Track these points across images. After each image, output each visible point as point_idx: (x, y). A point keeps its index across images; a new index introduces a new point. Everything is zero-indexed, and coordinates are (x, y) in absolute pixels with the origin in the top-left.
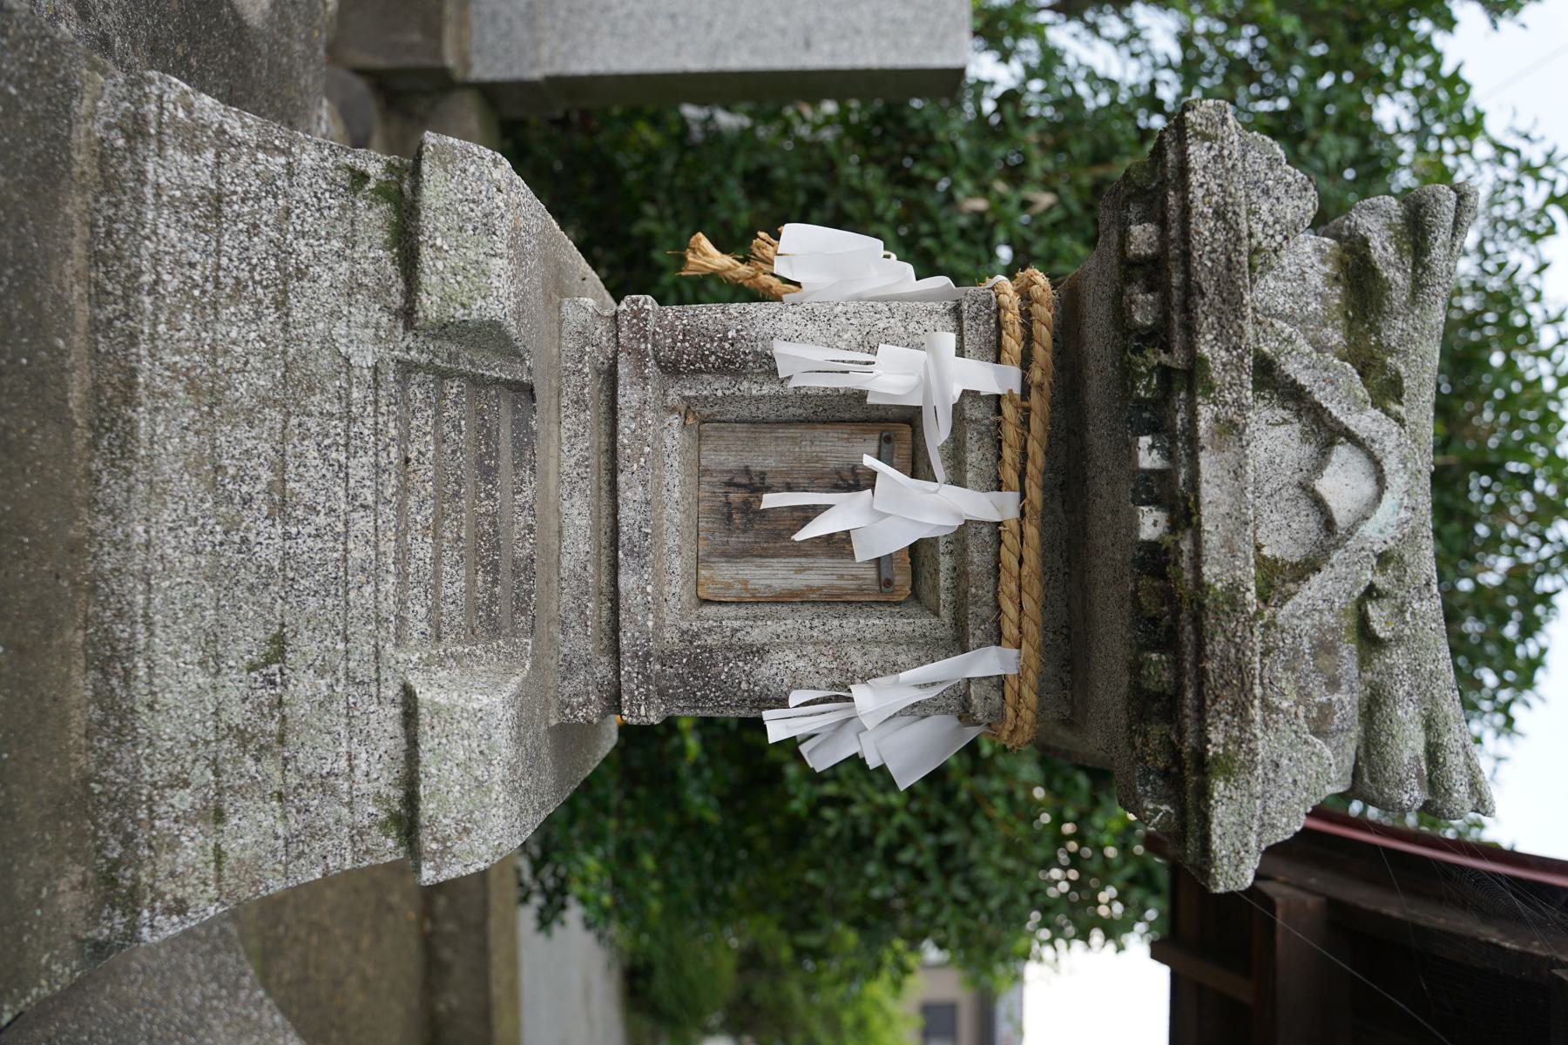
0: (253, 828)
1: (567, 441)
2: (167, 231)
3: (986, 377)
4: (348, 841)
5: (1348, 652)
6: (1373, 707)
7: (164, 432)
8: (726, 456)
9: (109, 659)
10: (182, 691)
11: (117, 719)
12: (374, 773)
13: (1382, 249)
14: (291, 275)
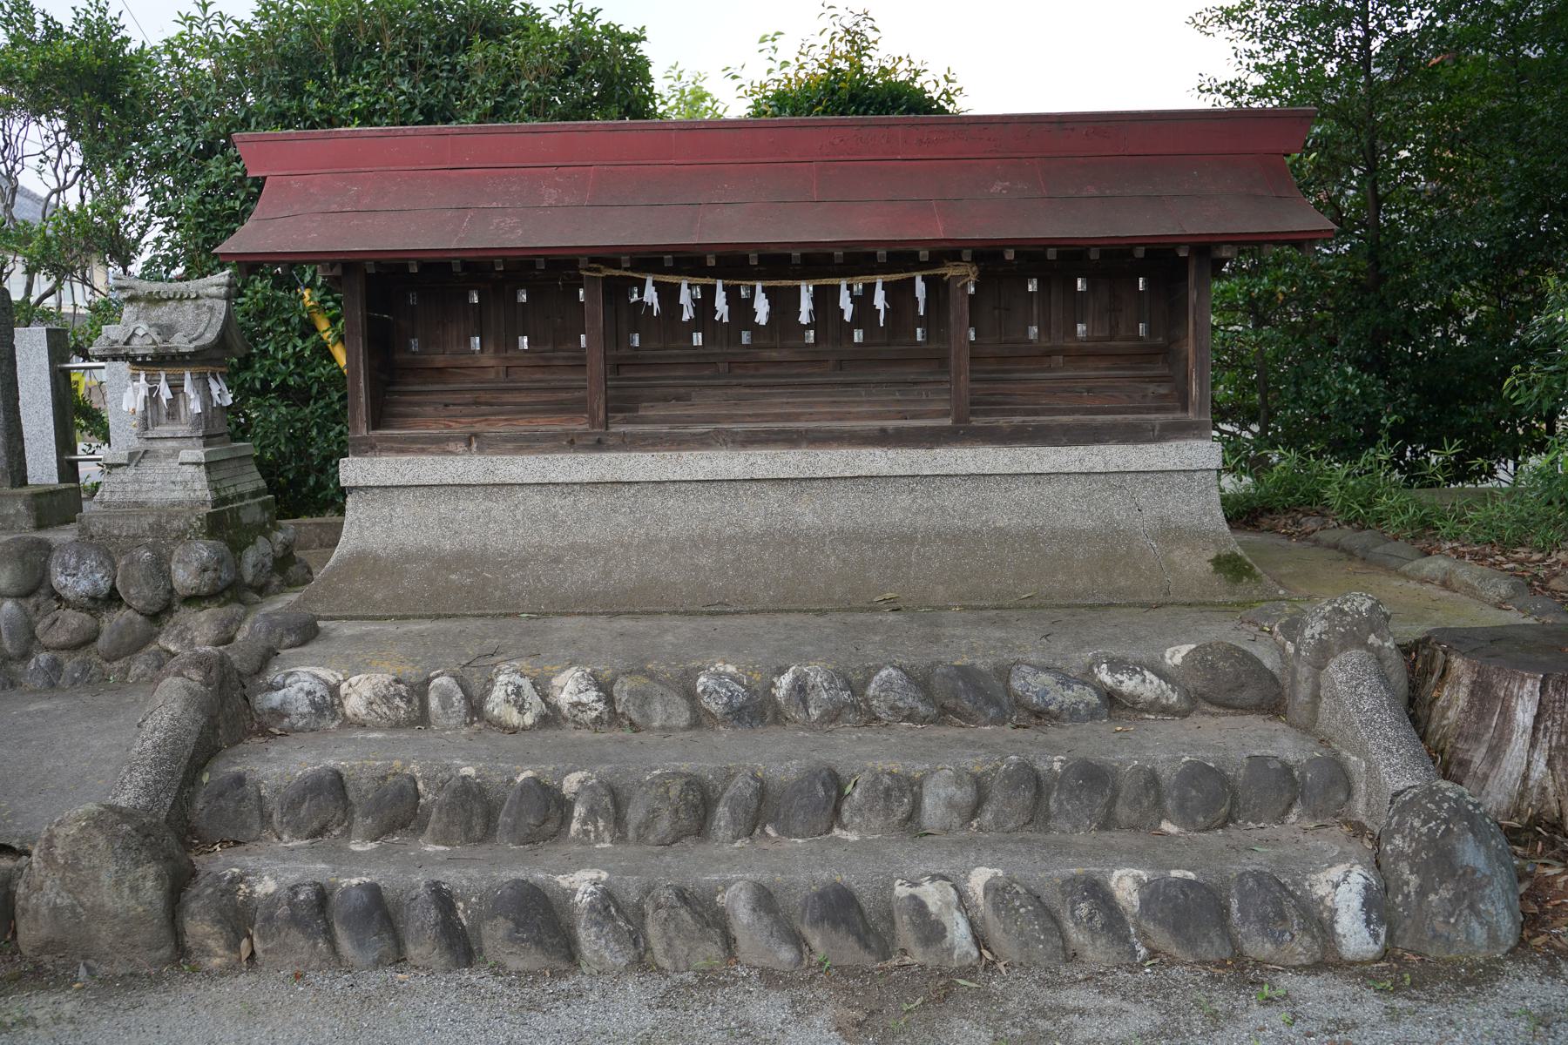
0: (198, 486)
1: (158, 445)
2: (115, 498)
3: (143, 377)
4: (201, 473)
5: (200, 302)
6: (210, 297)
7: (142, 497)
8: (164, 420)
9: (173, 505)
10: (178, 494)
11: (181, 503)
12: (192, 469)
13: (125, 295)
14: (122, 482)
